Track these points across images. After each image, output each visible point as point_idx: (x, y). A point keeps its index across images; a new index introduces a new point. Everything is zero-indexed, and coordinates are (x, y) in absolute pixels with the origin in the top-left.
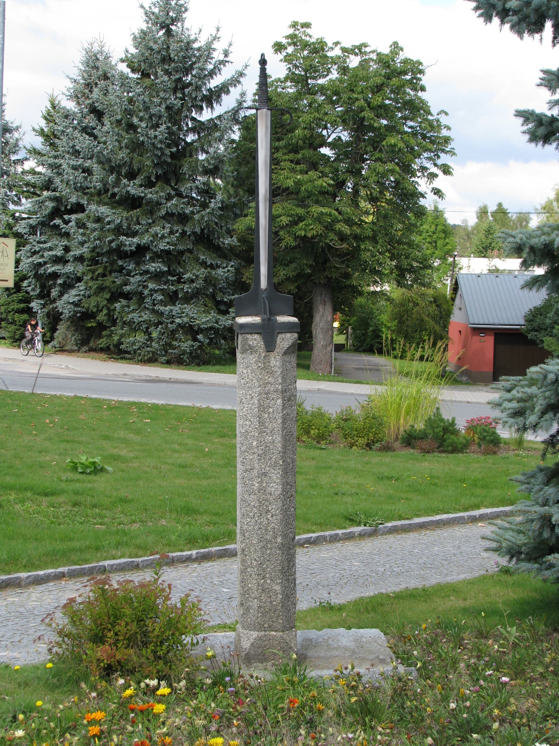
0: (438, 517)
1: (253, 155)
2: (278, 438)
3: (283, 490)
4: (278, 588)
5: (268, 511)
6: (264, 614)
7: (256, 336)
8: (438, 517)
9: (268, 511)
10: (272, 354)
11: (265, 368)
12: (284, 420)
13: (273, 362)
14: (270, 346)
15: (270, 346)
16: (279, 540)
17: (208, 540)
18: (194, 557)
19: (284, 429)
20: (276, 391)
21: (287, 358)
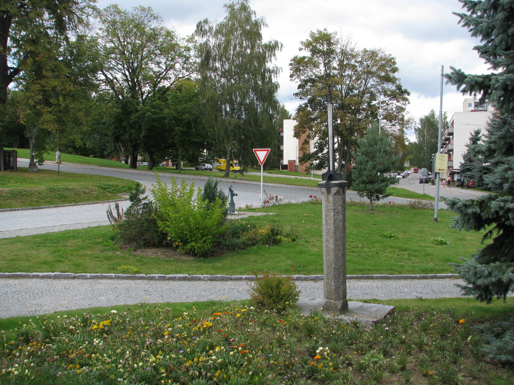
0: (18, 273)
1: (339, 184)
2: (332, 227)
3: (335, 247)
4: (333, 284)
5: (329, 254)
6: (328, 293)
7: (324, 188)
8: (18, 273)
9: (329, 254)
10: (330, 195)
11: (327, 200)
12: (335, 220)
13: (330, 198)
14: (329, 192)
15: (329, 192)
16: (333, 266)
17: (432, 271)
18: (89, 277)
19: (334, 224)
20: (331, 209)
21: (336, 197)
